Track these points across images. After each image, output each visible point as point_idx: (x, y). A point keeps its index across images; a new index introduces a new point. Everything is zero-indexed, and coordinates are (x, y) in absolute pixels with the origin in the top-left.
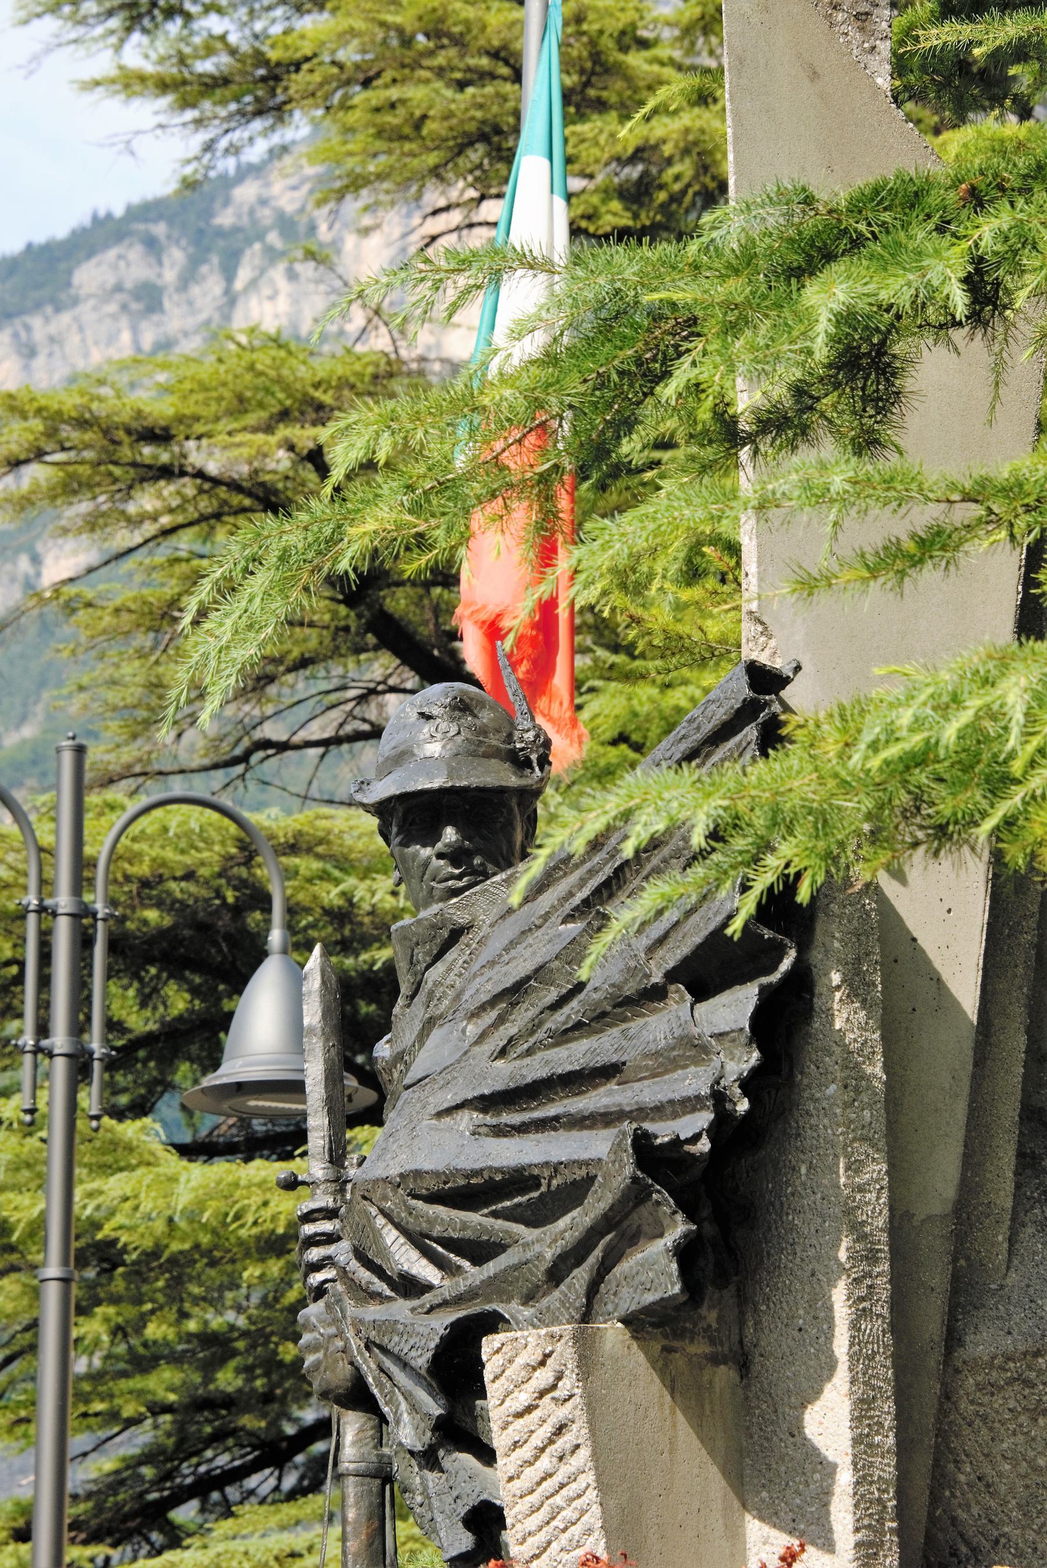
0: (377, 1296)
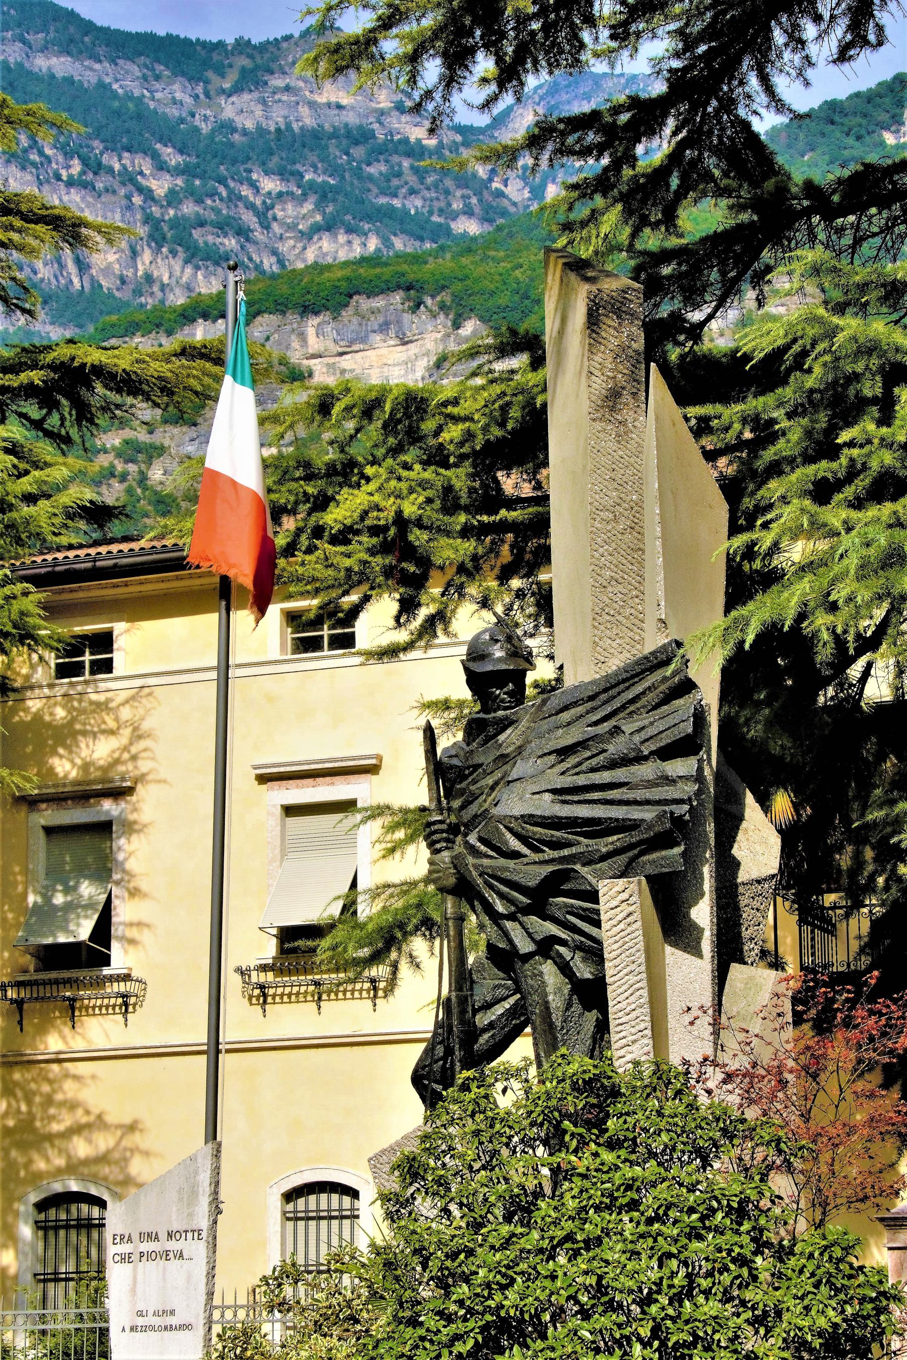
0: (491, 857)
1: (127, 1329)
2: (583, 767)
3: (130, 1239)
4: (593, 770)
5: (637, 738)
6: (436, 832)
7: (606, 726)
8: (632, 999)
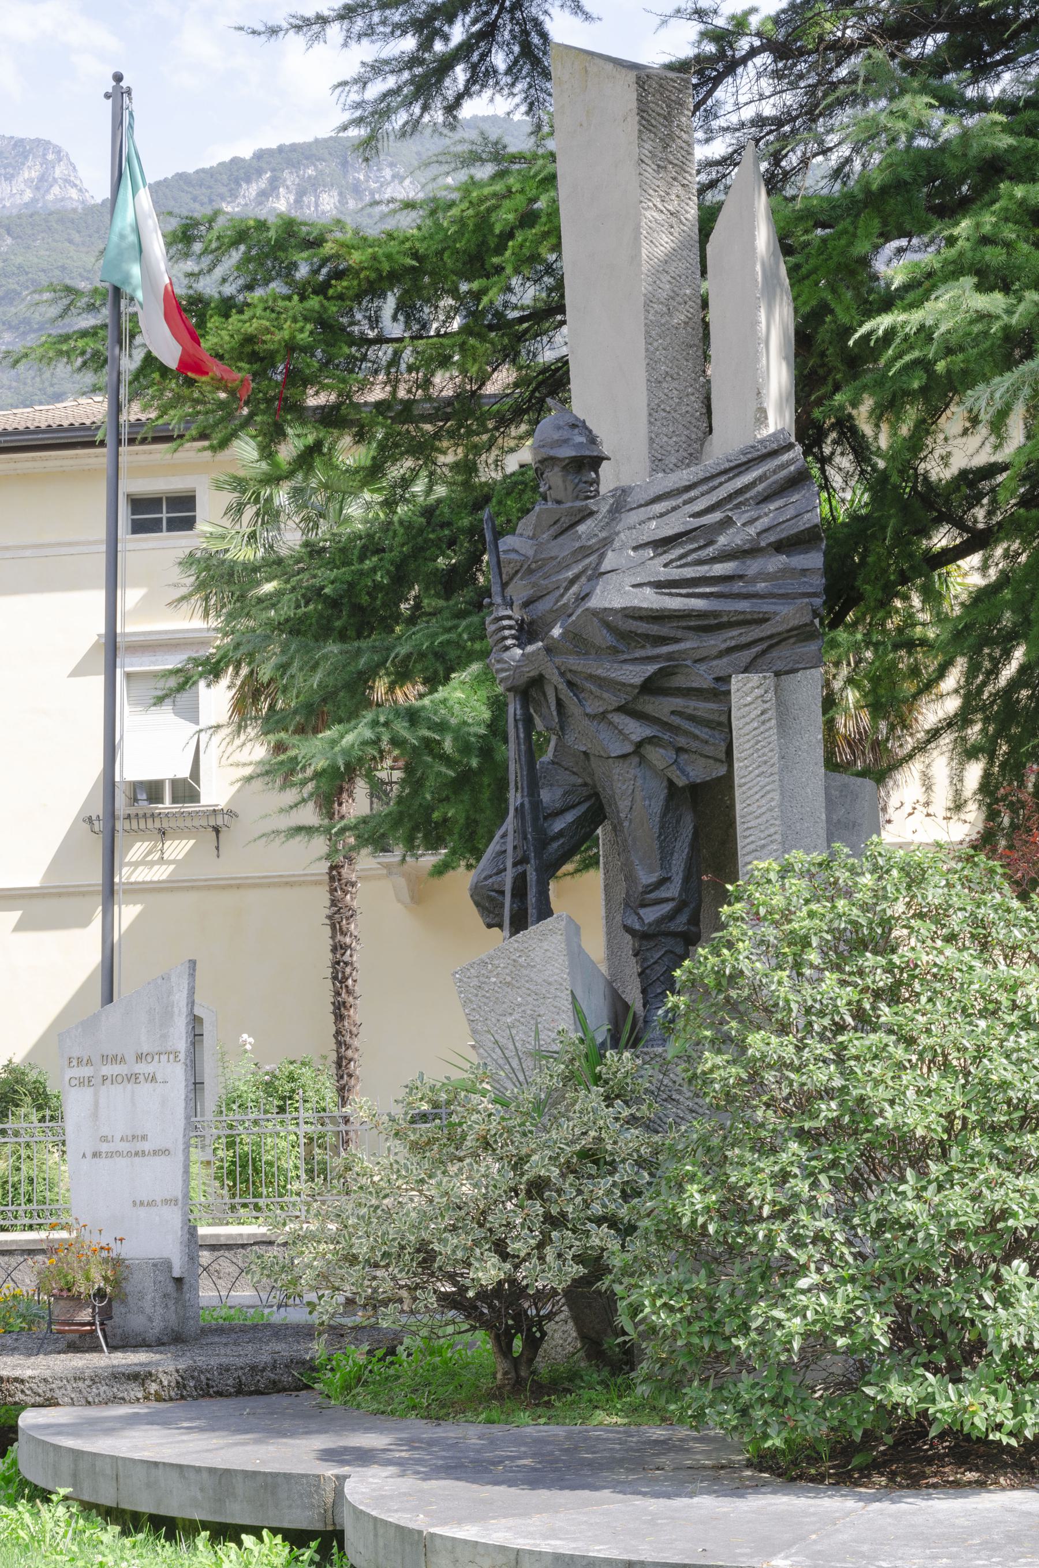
1: (89, 1155)
2: (689, 559)
3: (89, 1062)
4: (700, 562)
5: (752, 531)
6: (504, 628)
7: (717, 516)
8: (763, 801)
